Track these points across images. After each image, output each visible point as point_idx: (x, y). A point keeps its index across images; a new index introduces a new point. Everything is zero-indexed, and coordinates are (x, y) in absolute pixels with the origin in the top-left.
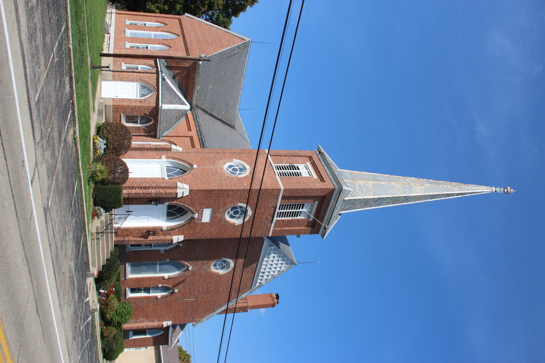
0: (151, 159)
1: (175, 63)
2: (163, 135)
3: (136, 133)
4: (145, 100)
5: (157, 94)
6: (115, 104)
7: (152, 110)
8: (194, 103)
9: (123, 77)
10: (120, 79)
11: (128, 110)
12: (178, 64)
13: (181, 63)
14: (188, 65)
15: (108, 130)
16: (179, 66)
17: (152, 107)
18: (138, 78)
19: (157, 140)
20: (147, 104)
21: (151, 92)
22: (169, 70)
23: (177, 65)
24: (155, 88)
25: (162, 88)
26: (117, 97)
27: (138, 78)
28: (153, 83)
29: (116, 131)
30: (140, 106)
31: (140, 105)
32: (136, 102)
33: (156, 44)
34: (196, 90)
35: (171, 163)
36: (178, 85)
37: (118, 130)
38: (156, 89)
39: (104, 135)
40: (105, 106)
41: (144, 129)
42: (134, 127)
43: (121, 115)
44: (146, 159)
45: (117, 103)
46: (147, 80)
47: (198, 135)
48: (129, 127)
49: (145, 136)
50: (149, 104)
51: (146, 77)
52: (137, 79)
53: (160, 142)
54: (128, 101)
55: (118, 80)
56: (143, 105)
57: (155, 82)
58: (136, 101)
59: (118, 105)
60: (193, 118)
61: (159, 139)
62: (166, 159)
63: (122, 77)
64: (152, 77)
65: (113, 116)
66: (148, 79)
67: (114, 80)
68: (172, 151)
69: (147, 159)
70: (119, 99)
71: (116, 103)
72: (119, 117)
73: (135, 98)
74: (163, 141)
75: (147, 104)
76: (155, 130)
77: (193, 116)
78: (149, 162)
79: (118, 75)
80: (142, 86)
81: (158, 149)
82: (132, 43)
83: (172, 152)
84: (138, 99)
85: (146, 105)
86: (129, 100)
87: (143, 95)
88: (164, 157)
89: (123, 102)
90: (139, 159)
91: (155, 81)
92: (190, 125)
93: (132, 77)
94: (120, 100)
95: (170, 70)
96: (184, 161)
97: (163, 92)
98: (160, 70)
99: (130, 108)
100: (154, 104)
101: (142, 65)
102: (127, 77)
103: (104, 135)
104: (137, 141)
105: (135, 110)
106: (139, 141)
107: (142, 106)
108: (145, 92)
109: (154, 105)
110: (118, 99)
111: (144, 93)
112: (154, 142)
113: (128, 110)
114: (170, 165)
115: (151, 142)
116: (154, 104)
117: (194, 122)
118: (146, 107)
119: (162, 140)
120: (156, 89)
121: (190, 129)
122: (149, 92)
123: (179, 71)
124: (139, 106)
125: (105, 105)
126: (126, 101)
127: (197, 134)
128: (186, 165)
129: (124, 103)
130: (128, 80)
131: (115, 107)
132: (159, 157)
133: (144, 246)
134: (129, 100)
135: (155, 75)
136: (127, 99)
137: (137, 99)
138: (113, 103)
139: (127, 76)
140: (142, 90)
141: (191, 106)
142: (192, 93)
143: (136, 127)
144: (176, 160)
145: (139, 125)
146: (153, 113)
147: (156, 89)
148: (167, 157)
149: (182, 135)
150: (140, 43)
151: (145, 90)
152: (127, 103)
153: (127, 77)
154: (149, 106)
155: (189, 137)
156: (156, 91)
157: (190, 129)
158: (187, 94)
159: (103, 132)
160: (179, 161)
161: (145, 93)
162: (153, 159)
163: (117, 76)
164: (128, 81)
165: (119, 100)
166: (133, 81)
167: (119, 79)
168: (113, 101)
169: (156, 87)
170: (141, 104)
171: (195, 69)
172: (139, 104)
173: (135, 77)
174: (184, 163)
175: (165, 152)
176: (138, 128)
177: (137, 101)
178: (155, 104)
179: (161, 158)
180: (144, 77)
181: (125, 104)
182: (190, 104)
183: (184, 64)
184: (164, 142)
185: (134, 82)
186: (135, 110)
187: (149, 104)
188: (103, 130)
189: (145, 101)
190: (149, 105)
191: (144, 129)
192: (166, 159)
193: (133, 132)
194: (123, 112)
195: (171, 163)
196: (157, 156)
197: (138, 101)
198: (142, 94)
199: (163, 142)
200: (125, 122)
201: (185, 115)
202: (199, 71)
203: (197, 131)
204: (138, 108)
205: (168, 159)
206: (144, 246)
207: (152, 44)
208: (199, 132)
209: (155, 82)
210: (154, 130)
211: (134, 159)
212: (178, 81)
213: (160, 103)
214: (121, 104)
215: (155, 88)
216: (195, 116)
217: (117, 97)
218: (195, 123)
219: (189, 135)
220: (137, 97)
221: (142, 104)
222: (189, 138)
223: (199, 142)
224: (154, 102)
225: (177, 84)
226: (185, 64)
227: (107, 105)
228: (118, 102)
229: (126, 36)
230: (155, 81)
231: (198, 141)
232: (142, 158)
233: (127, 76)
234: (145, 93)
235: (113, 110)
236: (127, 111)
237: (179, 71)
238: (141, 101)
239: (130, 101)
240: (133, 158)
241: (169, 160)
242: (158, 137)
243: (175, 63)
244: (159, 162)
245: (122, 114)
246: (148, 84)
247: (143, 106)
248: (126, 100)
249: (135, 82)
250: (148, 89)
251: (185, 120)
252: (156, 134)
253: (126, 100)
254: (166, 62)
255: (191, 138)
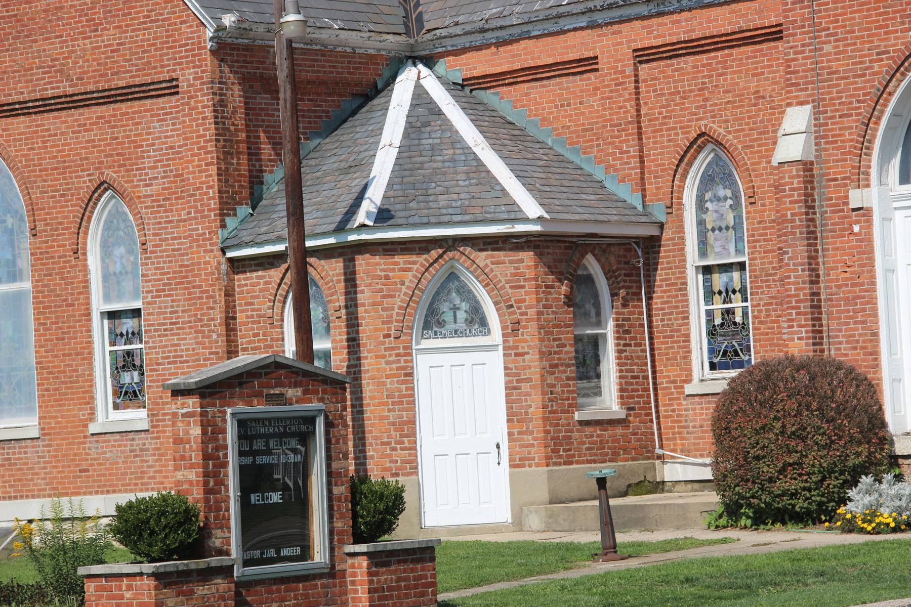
0: (871, 260)
1: (235, 161)
2: (638, 203)
3: (640, 345)
4: (504, 305)
5: (469, 249)
6: (538, 453)
7: (551, 269)
8: (393, 42)
9: (393, 424)
10: (405, 440)
11: (558, 389)
12: (237, 141)
13: (232, 128)
14: (237, 90)
15: (782, 471)
16: (243, 136)
17: (536, 267)
18: (393, 349)
19: (667, 234)
20: (528, 294)
21: (452, 276)
22: (265, 187)
23: (243, 147)
24: (435, 261)
25: (439, 224)
26: (498, 446)
27: (393, 349)
28: (409, 270)
29: (782, 433)
30: (541, 327)
31: (533, 327)
32: (521, 350)
33: (85, 266)
34: (344, 35)
35: (885, 160)
36: (319, 135)
37: (778, 425)
38: (440, 251)
39: (809, 490)
40: (556, 503)
41: (625, 306)
42: (619, 352)
43: (581, 423)
44: (874, 284)
45: (533, 445)
46: (398, 302)
47: (620, 22)
48: (620, 377)
49: (649, 298)
50: (523, 287)
51: (384, 309)
52: (398, 355)
53: (681, 220)
54: (519, 388)
55: (410, 449)
56: (532, 312)
57: (405, 263)
58: (512, 352)
59: (545, 438)
60: (493, 49)
61: (662, 226)
62: (868, 186)
63: (396, 430)
64: (380, 277)
65: (589, 462)
66: (394, 296)
67: (416, 468)
68: (812, 158)
69: (874, 277)
70: (510, 434)
71: (533, 450)
72: (588, 430)
73: (496, 361)
74: (674, 206)
75: (527, 293)
76: (626, 244)
77: (478, 48)
78: (887, 270)
79: (388, 452)
80: (427, 326)
81: (812, 229)
82: (92, 398)
83: (817, 157)
84: (504, 341)
85: (530, 299)
86: (515, 388)
87: (477, 319)
88: (856, 198)
89: (526, 413)
90: (876, 315)
91: (397, 259)
92: (550, 61)
93: (387, 377)
94: (515, 431)
95: (262, 183)
96: (882, 94)
97: (459, 218)
98: (331, 240)
99: (549, 382)
100: (522, 261)
101: (283, 333)
102: (393, 403)
103: (809, 490)
104: (688, 336)
105: (555, 353)
106: (688, 324)
107: (538, 319)
108: (455, 309)
109: (527, 257)
110: (511, 440)
111: (461, 315)
112: (683, 249)
113: (558, 389)
114: (892, 163)
115: (684, 267)
116: (522, 261)
117: (523, 44)
118: (539, 300)
119: (670, 207)
120: (441, 256)
121: (588, 64)
122: (453, 285)
123: (262, 135)
124: (540, 333)
125: (551, 503)
126: (519, 401)
127: (616, 27)
128: (903, 84)
129: (530, 411)
130: (408, 400)
131: (553, 451)
132: (857, 222)
133: (745, 304)
134: (515, 388)
135: (362, 262)
136: (507, 395)
137: (505, 348)
138: (537, 465)
139: (387, 404)
140: (451, 326)
141: (408, 58)
142: (352, 57)
143: (618, 345)
144: (874, 136)
145: (610, 329)
146: (560, 261)
147: (441, 256)
148: (861, 178)
149: (630, 106)
150: (91, 353)
151: (445, 307)
152: (528, 394)
153: (393, 403)
154: (538, 286)
155: (636, 69)
156: (450, 254)
157: (588, 64)
158: (356, 85)
159: (794, 495)
160: (879, 118)
161: (464, 306)
162: (872, 251)
163: (391, 456)
164: (413, 395)
165: (520, 433)
166: (411, 375)
167: (406, 445)
168: (523, 466)
169: (434, 254)
170: (526, 327)
171: (247, 48)
172: (530, 336)
173: (387, 363)
174: (890, 94)
175: (824, 193)
176: (622, 332)
177: (517, 348)
178: (522, 255)
179: (864, 213)
180: (381, 316)
181: (534, 402)
182: (397, 64)
183: (235, 112)
184: (681, 198)
185: (412, 368)
186: (555, 353)
187: (523, 287)
188: (783, 495)
189: (512, 306)
190: (529, 286)
191: (625, 306)
192: (868, 186)
193: (638, 357)
194: (568, 412)
195: (885, 160)
196: (856, 228)
197: (511, 339)
198: (470, 322)
199: (681, 204)
200: (598, 398)
201: (467, 89)
202: (261, 29)
203: (593, 26)
204: (549, 340)
205: (868, 174)
206: (745, 304)
207: (87, 287)
208: (600, 17)
209: (405, 263)
210: (622, 253)
211: (878, 341)
212: (306, 139)
213: (520, 228)
214: (536, 424)
215: (435, 261)
216: (478, 39)
217: (498, 446)
218: (530, 38)
219: (629, 71)
220: (492, 348)
221: (528, 320)
222: (640, 67)
223: (675, 17)
224: (511, 262)
225: (317, 141)
226: (230, 108)
227: (549, 491)
228: (529, 439)
229: (35, 433)
230: (397, 264)
231: (666, 19)
232: (873, 301)
233: (387, 404)
234: (464, 306)
235: (565, 463)
236: (563, 391)
237: (262, 135)
238: (513, 329)
239: (518, 381)
240: (877, 346)
241: (874, 172)
242: (655, 232)
243: (235, 161)
244: (884, 219)
245: (577, 416)
246: (420, 298)
247: (539, 313)
248: (514, 401)
249: (412, 361)
250: (437, 293)
251: (505, 89)
252: (638, 240)
253: (514, 401)
254: (235, 209)
255: (644, 56)
